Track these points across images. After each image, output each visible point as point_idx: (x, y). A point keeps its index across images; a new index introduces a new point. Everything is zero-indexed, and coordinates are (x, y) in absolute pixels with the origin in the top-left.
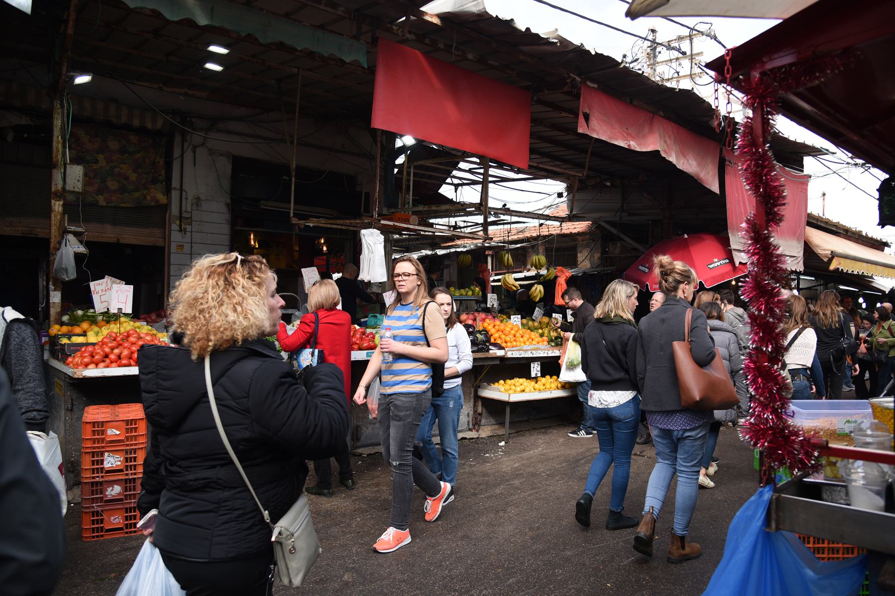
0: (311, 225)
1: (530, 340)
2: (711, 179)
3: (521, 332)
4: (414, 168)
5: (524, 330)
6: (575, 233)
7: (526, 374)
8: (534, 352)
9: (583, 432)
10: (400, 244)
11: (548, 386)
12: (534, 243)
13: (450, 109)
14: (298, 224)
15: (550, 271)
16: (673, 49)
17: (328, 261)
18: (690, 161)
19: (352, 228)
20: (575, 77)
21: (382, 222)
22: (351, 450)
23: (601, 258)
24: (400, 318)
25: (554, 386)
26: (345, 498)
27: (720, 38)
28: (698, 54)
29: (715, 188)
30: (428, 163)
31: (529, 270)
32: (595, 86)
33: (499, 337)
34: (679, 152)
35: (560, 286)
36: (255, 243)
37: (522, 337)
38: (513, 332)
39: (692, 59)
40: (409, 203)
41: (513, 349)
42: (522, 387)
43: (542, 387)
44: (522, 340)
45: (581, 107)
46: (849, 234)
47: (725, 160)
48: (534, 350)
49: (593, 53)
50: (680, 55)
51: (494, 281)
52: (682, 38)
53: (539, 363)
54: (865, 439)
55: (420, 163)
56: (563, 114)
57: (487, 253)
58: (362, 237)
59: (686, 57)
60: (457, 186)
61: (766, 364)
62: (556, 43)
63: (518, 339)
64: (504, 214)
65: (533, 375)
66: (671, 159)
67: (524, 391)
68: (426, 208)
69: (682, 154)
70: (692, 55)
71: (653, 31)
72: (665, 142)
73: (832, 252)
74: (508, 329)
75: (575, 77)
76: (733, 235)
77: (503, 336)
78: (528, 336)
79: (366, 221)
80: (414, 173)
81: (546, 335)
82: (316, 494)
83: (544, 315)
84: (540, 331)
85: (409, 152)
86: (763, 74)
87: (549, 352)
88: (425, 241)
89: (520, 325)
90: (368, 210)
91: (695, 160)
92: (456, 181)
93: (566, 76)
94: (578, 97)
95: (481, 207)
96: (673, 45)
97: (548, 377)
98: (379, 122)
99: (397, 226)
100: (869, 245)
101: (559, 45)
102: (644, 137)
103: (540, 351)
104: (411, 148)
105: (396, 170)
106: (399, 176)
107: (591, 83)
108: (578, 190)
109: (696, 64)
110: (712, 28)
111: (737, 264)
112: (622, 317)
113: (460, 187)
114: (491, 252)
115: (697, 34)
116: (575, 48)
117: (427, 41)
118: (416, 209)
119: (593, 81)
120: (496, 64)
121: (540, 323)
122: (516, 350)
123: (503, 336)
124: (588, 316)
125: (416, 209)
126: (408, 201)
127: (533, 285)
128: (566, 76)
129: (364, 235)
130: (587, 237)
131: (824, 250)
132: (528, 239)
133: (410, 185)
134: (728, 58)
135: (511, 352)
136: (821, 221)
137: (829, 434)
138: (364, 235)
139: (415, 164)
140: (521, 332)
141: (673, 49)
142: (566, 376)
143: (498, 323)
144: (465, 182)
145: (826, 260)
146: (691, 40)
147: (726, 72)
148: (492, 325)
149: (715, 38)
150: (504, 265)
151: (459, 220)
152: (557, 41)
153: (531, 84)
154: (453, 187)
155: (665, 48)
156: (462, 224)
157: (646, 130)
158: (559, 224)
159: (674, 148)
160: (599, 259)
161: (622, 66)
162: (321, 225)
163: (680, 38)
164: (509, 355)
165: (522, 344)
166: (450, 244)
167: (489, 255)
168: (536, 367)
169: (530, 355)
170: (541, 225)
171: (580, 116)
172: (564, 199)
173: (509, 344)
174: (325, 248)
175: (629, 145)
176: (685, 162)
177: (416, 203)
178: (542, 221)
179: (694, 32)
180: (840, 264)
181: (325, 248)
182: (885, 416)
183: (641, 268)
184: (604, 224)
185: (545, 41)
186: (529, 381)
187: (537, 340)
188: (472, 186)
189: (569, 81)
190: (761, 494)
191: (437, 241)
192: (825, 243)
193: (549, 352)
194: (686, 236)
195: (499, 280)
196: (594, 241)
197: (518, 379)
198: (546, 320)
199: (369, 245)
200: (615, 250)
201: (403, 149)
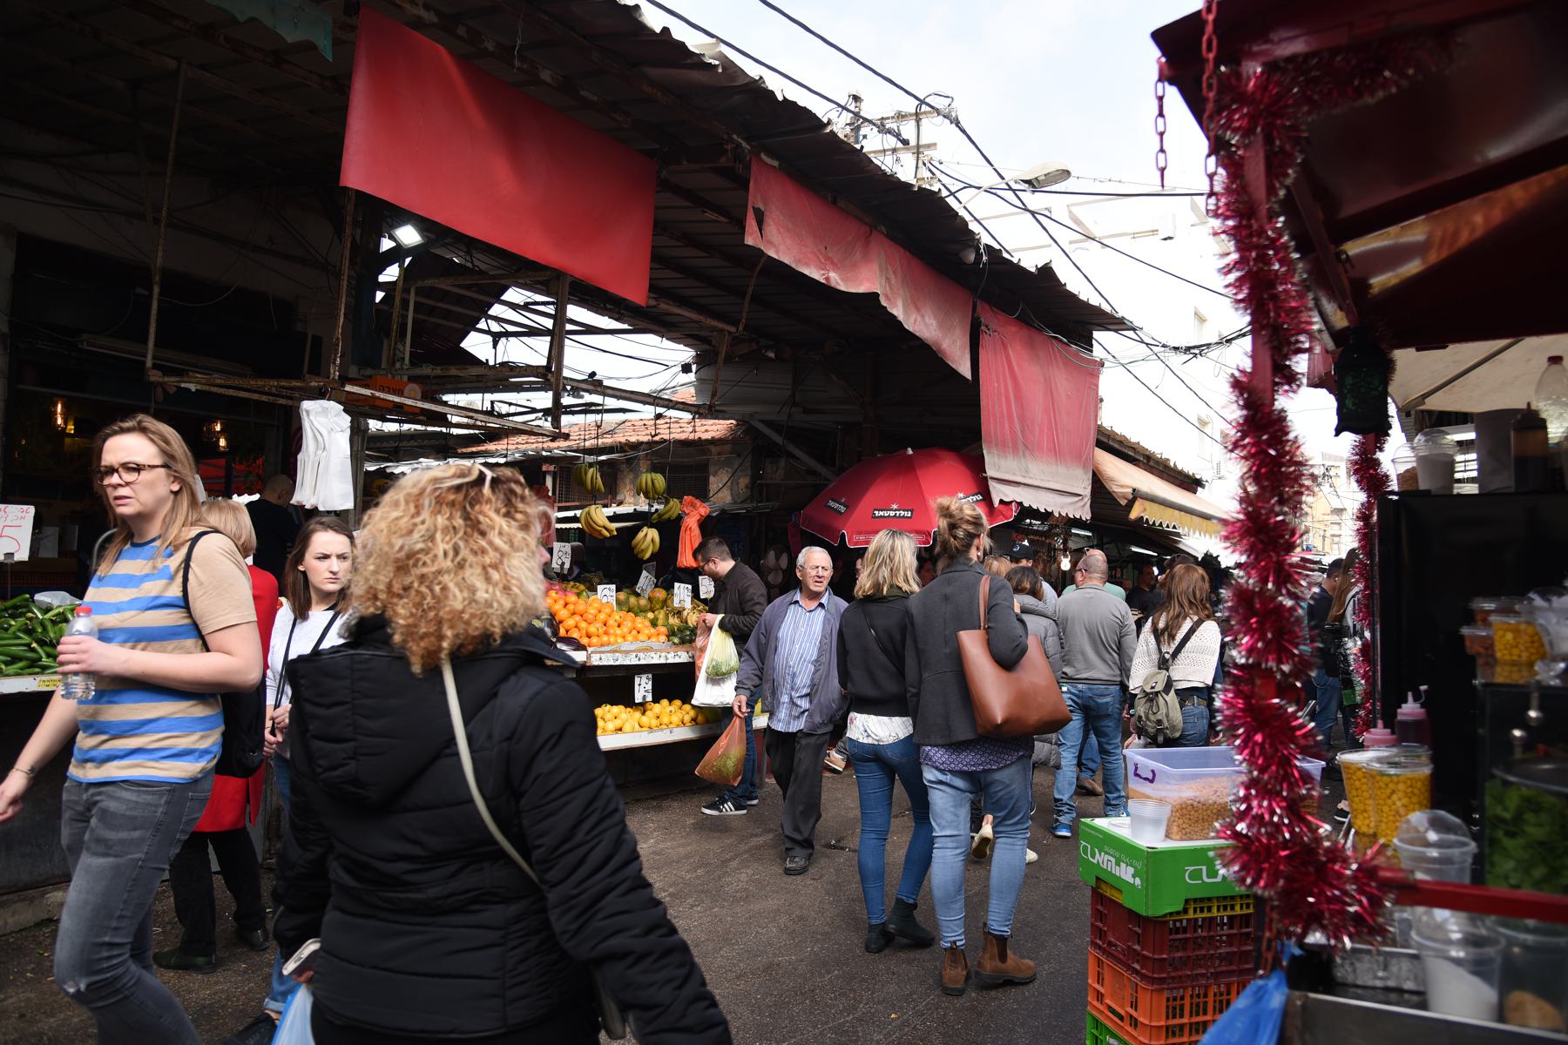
0: (193, 387)
1: (634, 632)
2: (958, 353)
3: (617, 617)
4: (417, 294)
5: (623, 614)
6: (707, 440)
7: (626, 698)
8: (641, 655)
9: (729, 806)
10: (378, 445)
11: (665, 720)
12: (631, 454)
13: (501, 172)
14: (162, 384)
15: (671, 503)
16: (889, 132)
17: (229, 469)
18: (927, 318)
19: (282, 401)
20: (740, 140)
21: (348, 388)
22: (264, 859)
23: (752, 486)
24: (129, 581)
25: (676, 719)
26: (245, 972)
27: (963, 124)
28: (929, 146)
29: (965, 370)
30: (444, 284)
31: (620, 504)
32: (775, 163)
33: (576, 627)
34: (909, 301)
35: (688, 532)
36: (66, 423)
37: (619, 626)
38: (602, 616)
39: (918, 153)
40: (403, 359)
41: (603, 649)
42: (618, 723)
43: (654, 722)
44: (618, 631)
45: (750, 198)
46: (1151, 463)
47: (980, 324)
48: (640, 651)
49: (780, 98)
50: (900, 145)
51: (560, 520)
52: (903, 117)
53: (650, 676)
54: (1424, 853)
55: (429, 282)
56: (710, 215)
57: (544, 468)
58: (304, 415)
59: (908, 149)
60: (496, 337)
61: (1276, 701)
62: (716, 66)
63: (612, 631)
64: (590, 392)
65: (638, 699)
66: (895, 312)
67: (620, 730)
68: (438, 371)
69: (914, 304)
70: (918, 146)
71: (856, 98)
72: (888, 279)
73: (1134, 490)
74: (592, 611)
75: (740, 140)
76: (989, 453)
77: (583, 625)
78: (629, 624)
79: (313, 384)
80: (416, 303)
81: (660, 622)
82: (176, 967)
83: (656, 586)
84: (651, 615)
85: (408, 260)
86: (1272, 67)
87: (669, 656)
88: (426, 442)
89: (614, 603)
90: (318, 369)
91: (935, 317)
92: (495, 327)
93: (725, 137)
94: (744, 185)
95: (549, 376)
96: (890, 125)
97: (665, 702)
98: (357, 174)
99: (379, 398)
100: (1177, 482)
101: (720, 70)
102: (854, 266)
103: (652, 654)
104: (412, 251)
105: (380, 295)
106: (386, 308)
107: (769, 157)
108: (729, 360)
109: (924, 164)
110: (953, 105)
111: (996, 503)
112: (900, 588)
113: (503, 340)
114: (552, 468)
115: (930, 112)
116: (747, 84)
117: (461, 31)
118: (418, 371)
119: (772, 155)
120: (595, 98)
121: (650, 599)
122: (608, 652)
123: (583, 625)
124: (749, 586)
125: (418, 371)
126: (402, 356)
127: (637, 529)
128: (725, 137)
129: (308, 412)
130: (728, 447)
131: (1122, 486)
132: (621, 447)
133: (406, 324)
134: (1211, 17)
135: (598, 656)
136: (1114, 440)
137: (1215, 811)
138: (308, 412)
139: (420, 284)
140: (617, 617)
141: (889, 132)
142: (706, 694)
143: (573, 598)
144: (511, 328)
145: (1123, 502)
146: (918, 121)
147: (1204, 46)
148: (561, 603)
149: (958, 124)
150: (587, 489)
151: (504, 401)
152: (717, 63)
153: (657, 146)
154: (489, 338)
155: (875, 129)
156: (504, 409)
157: (858, 255)
158: (691, 417)
159: (901, 292)
160: (747, 487)
161: (828, 131)
162: (214, 389)
163: (901, 116)
164: (596, 660)
165: (620, 640)
166: (474, 449)
167: (548, 472)
168: (643, 684)
169: (635, 662)
170: (659, 416)
171: (614, 322)
172: (691, 377)
173: (594, 640)
174: (222, 442)
175: (827, 279)
176: (919, 318)
177: (416, 360)
178: (660, 410)
179: (924, 108)
180: (1145, 510)
181: (222, 442)
182: (1380, 788)
183: (831, 504)
184: (761, 427)
185: (695, 60)
186: (629, 709)
187: (647, 631)
188: (525, 339)
189: (729, 147)
190: (1260, 996)
191: (451, 443)
192: (1124, 477)
193: (669, 656)
194: (910, 451)
195: (575, 519)
196: (739, 455)
197: (609, 706)
198: (661, 594)
199: (317, 434)
200: (776, 473)
201: (397, 254)
